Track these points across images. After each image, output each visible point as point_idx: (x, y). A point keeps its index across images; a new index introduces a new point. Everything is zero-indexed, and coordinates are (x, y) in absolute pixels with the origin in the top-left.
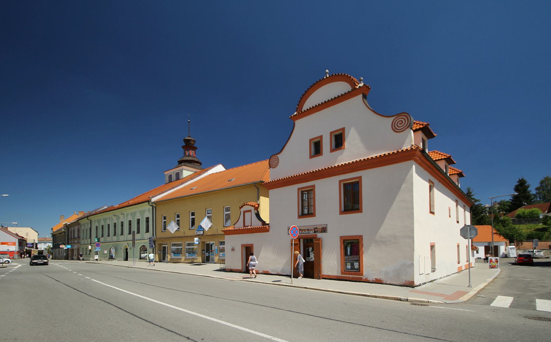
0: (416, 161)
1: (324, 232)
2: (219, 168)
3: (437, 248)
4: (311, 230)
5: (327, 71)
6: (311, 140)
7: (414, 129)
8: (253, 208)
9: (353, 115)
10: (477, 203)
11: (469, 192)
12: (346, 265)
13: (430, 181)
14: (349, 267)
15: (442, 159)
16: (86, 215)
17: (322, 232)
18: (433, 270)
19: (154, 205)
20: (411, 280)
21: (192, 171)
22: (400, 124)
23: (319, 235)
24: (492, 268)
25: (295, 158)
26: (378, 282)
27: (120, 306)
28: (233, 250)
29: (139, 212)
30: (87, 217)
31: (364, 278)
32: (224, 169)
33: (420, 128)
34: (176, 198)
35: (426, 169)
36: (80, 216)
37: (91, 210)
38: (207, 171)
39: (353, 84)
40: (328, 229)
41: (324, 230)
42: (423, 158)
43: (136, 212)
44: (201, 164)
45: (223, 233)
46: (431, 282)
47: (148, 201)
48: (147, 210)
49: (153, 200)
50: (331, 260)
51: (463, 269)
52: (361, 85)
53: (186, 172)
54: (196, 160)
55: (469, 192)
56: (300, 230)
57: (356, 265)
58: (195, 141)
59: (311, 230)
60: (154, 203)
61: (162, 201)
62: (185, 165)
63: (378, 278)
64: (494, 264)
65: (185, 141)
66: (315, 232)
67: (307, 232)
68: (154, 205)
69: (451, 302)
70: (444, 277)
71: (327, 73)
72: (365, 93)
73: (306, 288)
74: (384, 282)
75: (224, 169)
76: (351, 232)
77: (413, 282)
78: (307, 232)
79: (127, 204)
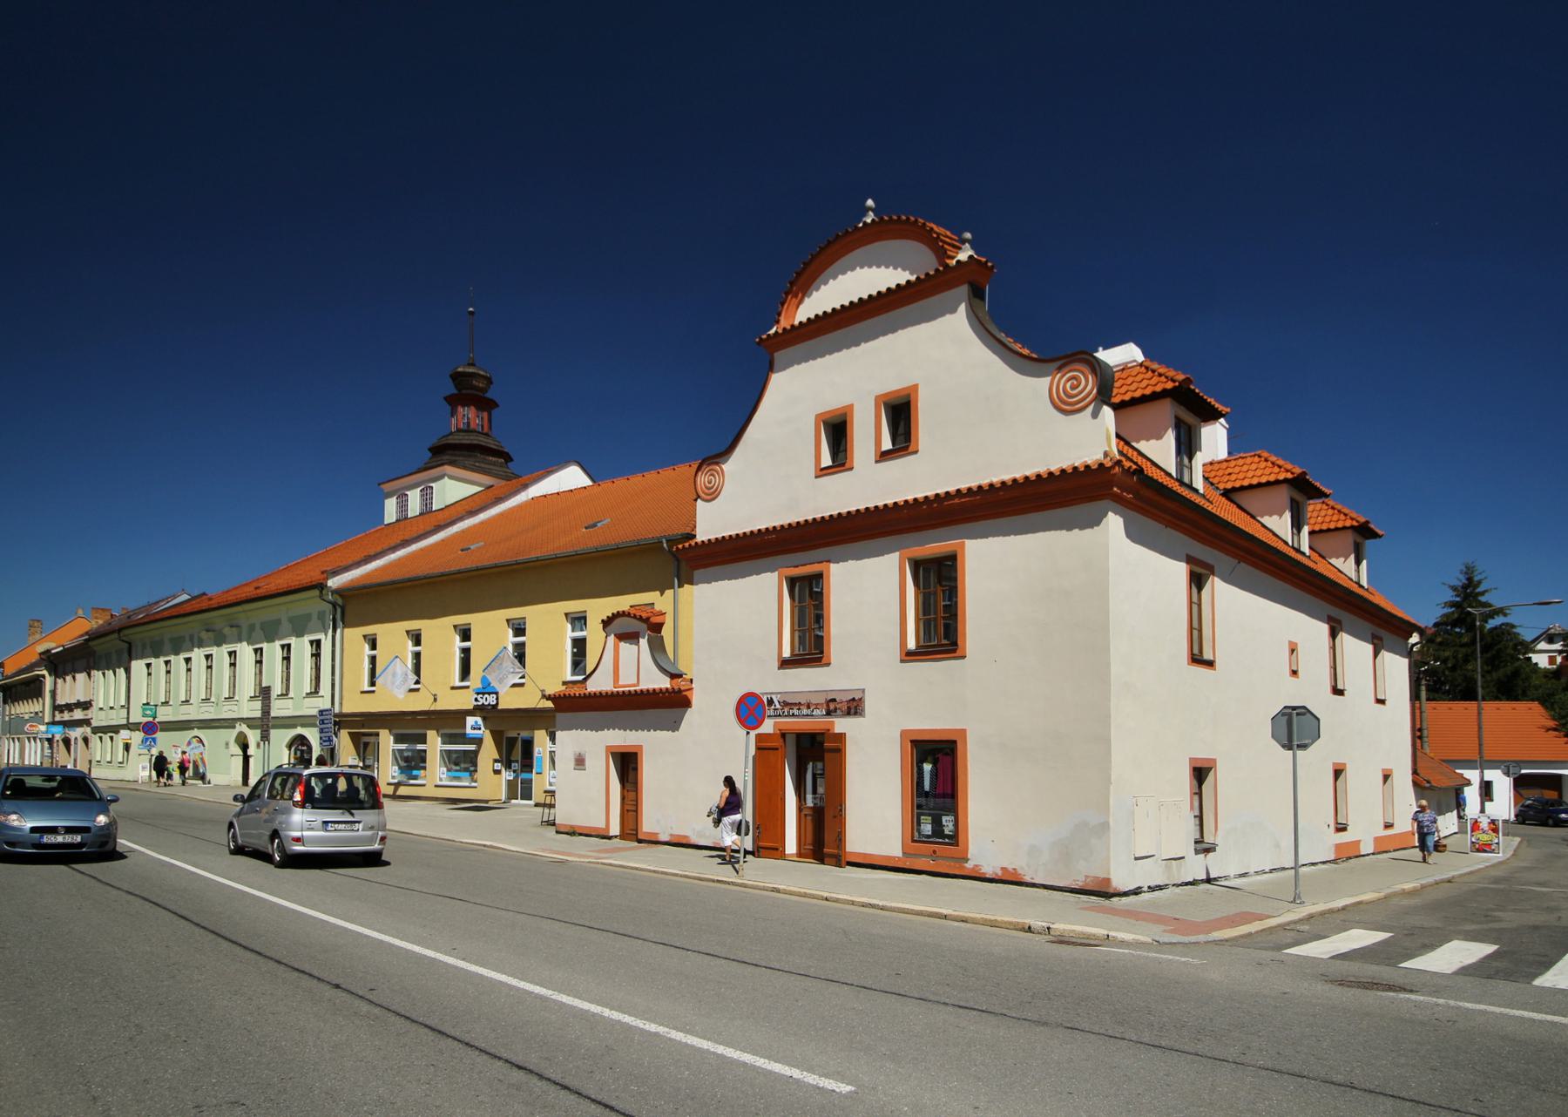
0: (1118, 499)
1: (856, 714)
2: (571, 478)
3: (1350, 774)
4: (817, 706)
5: (870, 202)
6: (818, 416)
7: (1116, 400)
8: (644, 626)
9: (945, 354)
10: (1492, 623)
11: (1470, 579)
12: (919, 824)
13: (1189, 560)
14: (927, 828)
15: (1277, 482)
16: (116, 624)
17: (849, 714)
18: (1204, 847)
19: (340, 601)
20: (1103, 875)
21: (479, 485)
22: (1073, 388)
23: (841, 725)
24: (1478, 850)
25: (767, 477)
26: (1010, 880)
27: (184, 913)
28: (580, 762)
29: (291, 620)
30: (120, 630)
31: (969, 865)
32: (588, 482)
33: (1165, 390)
34: (410, 580)
35: (1168, 524)
36: (95, 623)
37: (132, 606)
38: (525, 486)
39: (942, 254)
40: (868, 705)
41: (854, 707)
42: (1146, 493)
43: (278, 622)
44: (507, 458)
45: (550, 704)
46: (1187, 884)
47: (321, 586)
48: (315, 617)
49: (333, 583)
50: (875, 808)
51: (1367, 847)
52: (963, 256)
53: (451, 489)
54: (490, 443)
55: (1470, 579)
56: (785, 704)
57: (948, 822)
58: (489, 381)
59: (817, 706)
60: (337, 592)
61: (365, 587)
62: (452, 463)
63: (1010, 867)
64: (1484, 838)
65: (457, 377)
66: (829, 713)
67: (805, 711)
68: (340, 601)
69: (1193, 939)
70: (1264, 872)
71: (870, 209)
72: (975, 284)
73: (778, 891)
74: (1027, 879)
75: (585, 481)
76: (933, 722)
77: (1108, 881)
78: (805, 711)
79: (249, 592)
